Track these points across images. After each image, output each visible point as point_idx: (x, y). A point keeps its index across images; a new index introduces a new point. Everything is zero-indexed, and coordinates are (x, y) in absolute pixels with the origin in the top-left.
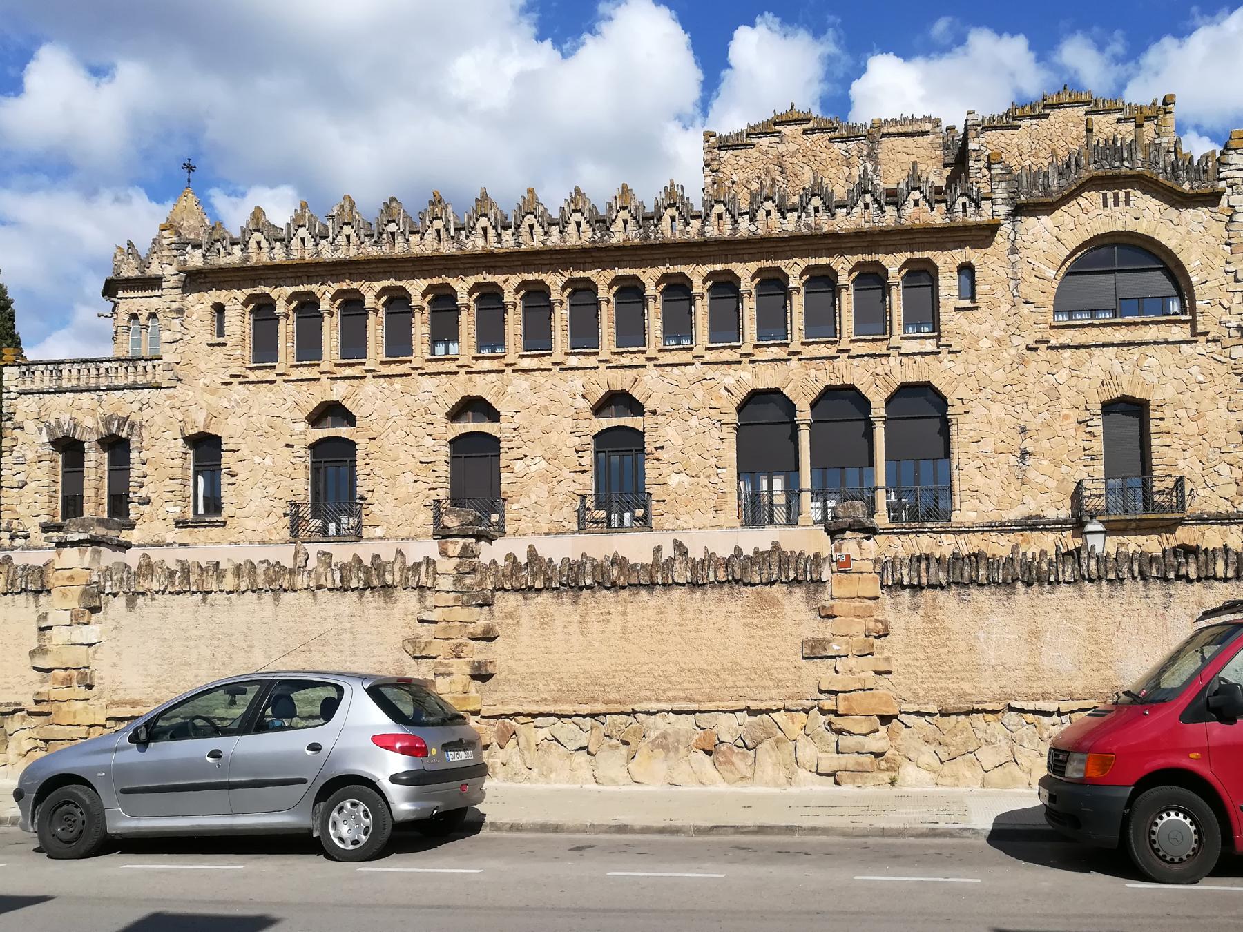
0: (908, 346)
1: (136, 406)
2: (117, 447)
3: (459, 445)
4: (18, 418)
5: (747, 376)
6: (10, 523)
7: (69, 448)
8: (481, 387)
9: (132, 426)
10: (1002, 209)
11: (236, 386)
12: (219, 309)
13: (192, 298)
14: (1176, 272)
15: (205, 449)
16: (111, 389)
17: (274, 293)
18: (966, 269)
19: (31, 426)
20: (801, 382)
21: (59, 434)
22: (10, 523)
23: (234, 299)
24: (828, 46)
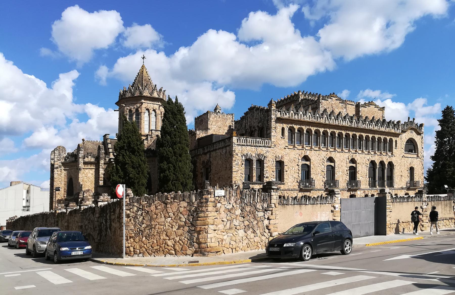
0: (338, 151)
1: (265, 152)
2: (261, 162)
3: (351, 168)
4: (236, 152)
5: (303, 152)
6: (235, 182)
7: (249, 162)
8: (308, 153)
9: (265, 157)
10: (400, 131)
11: (287, 149)
12: (283, 129)
13: (278, 124)
14: (415, 146)
15: (280, 164)
16: (260, 146)
17: (312, 128)
18: (396, 141)
19: (239, 155)
20: (377, 159)
21: (248, 158)
22: (235, 182)
23: (286, 127)
24: (158, 39)
